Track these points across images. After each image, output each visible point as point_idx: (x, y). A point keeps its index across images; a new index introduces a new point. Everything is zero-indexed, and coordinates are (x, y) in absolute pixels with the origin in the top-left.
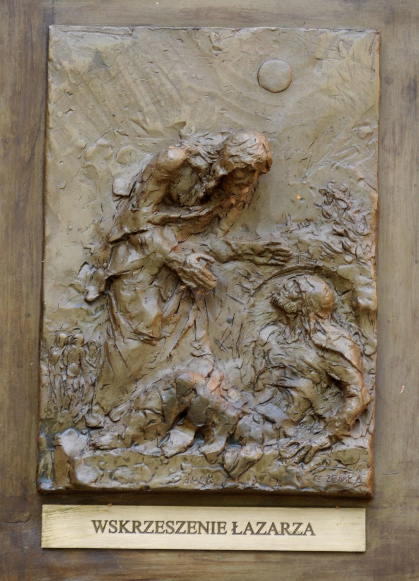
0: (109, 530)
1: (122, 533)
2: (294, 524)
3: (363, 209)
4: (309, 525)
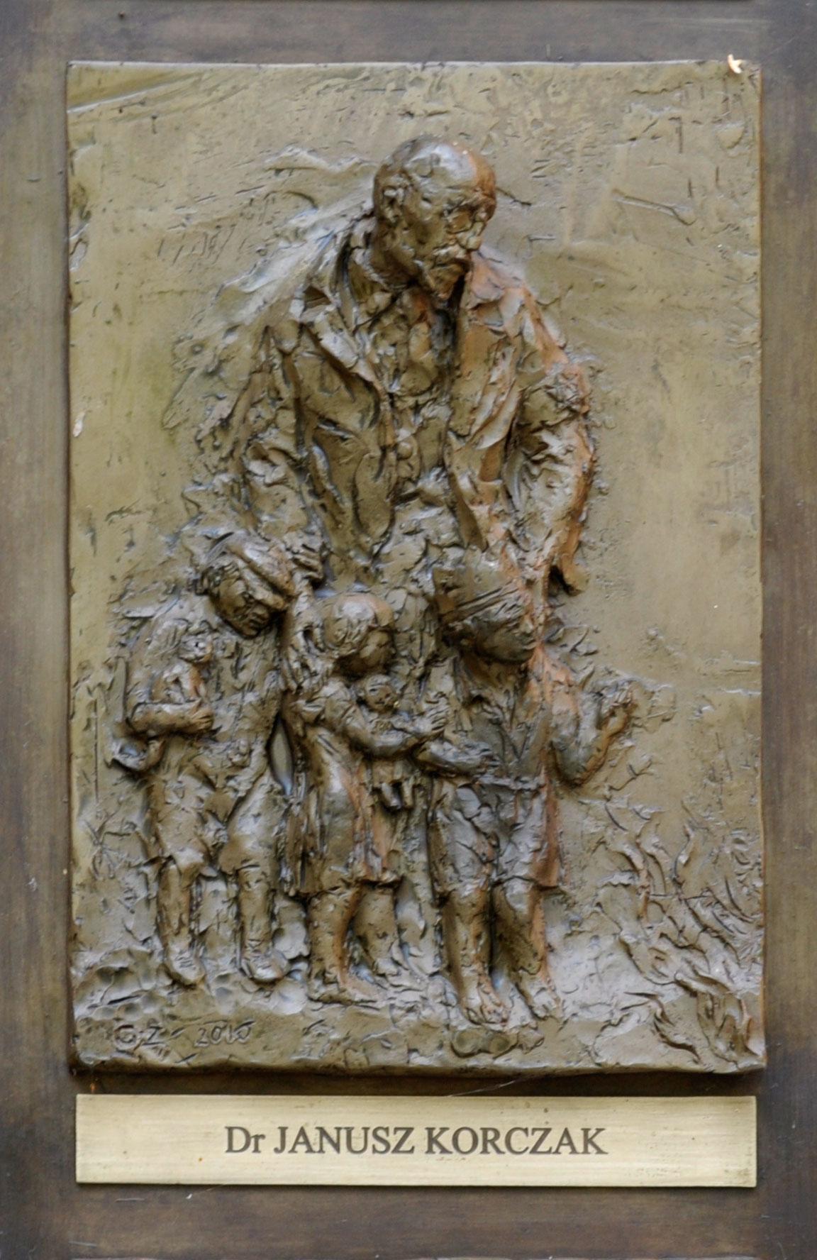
0: (374, 1146)
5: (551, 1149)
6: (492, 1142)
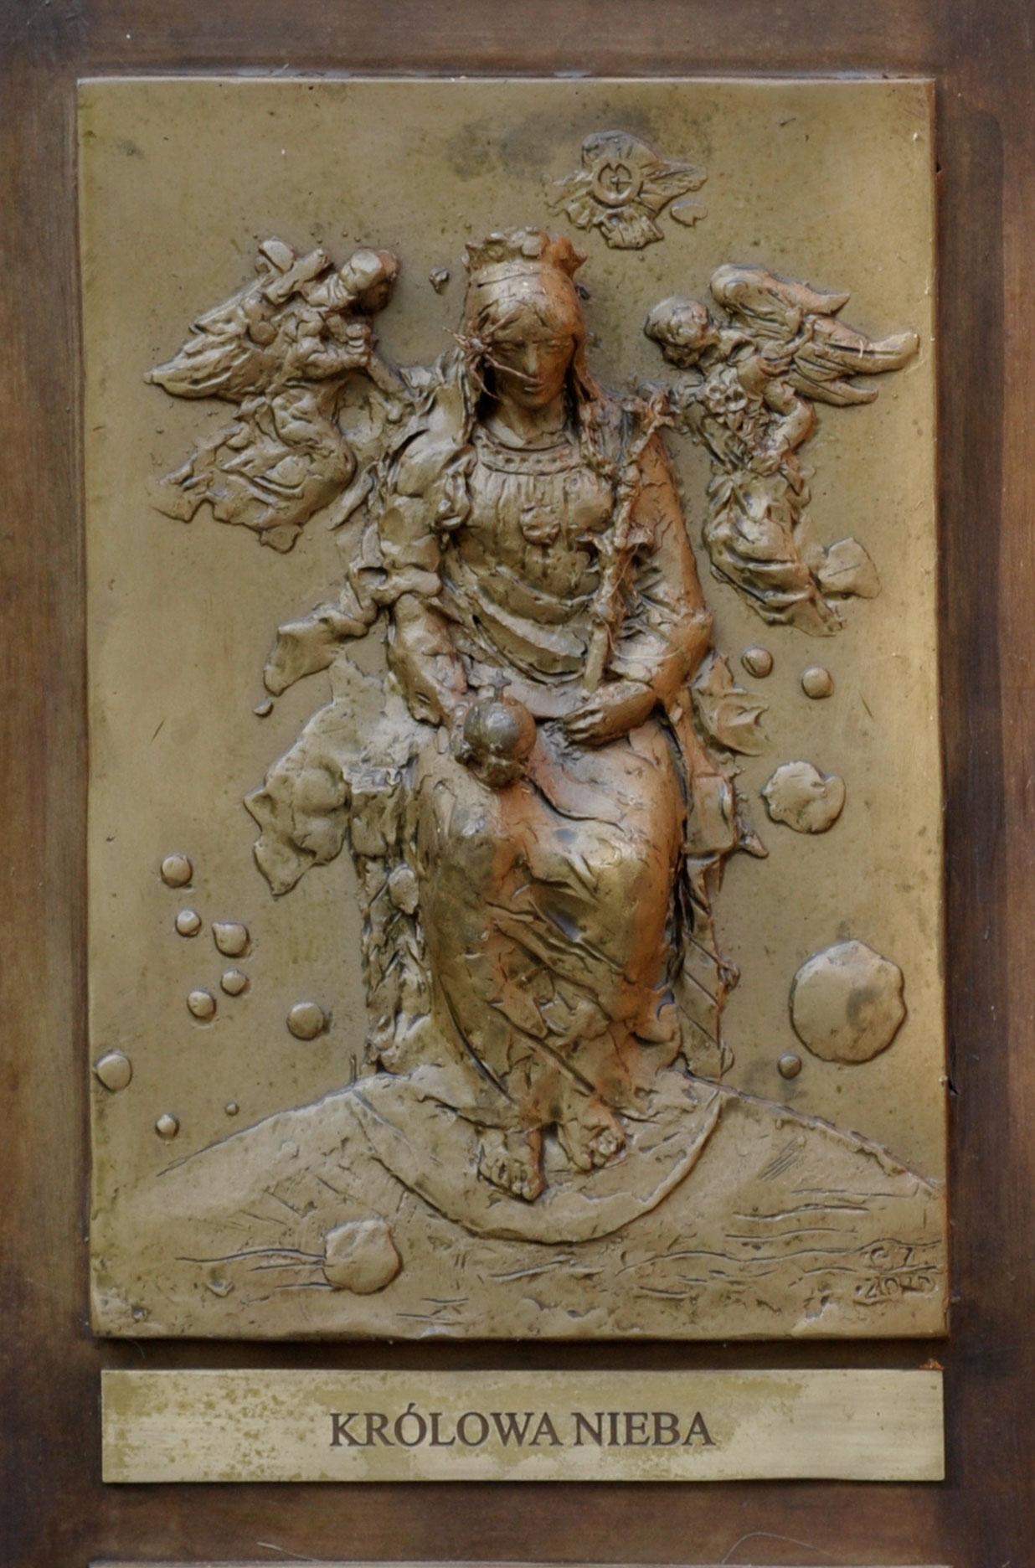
1: (340, 1445)
4: (546, 1418)
6: (379, 1430)
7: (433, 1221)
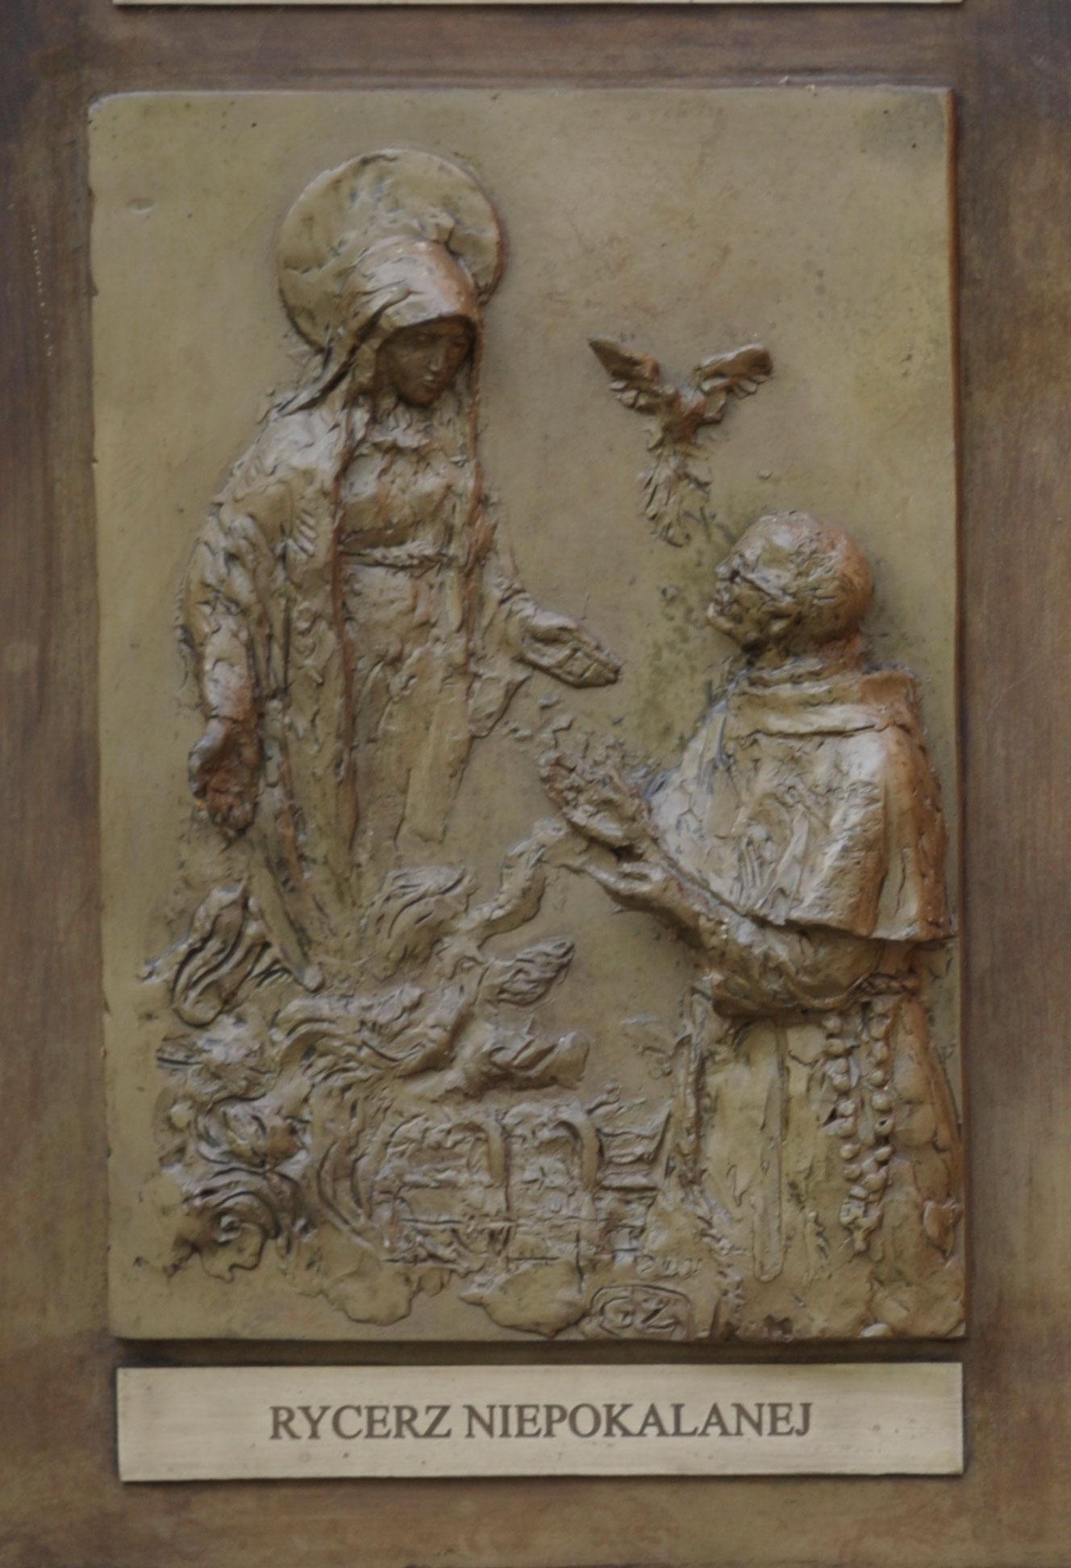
1: (403, 1437)
2: (429, 1408)
3: (612, 1099)
5: (696, 1429)
7: (775, 1237)
